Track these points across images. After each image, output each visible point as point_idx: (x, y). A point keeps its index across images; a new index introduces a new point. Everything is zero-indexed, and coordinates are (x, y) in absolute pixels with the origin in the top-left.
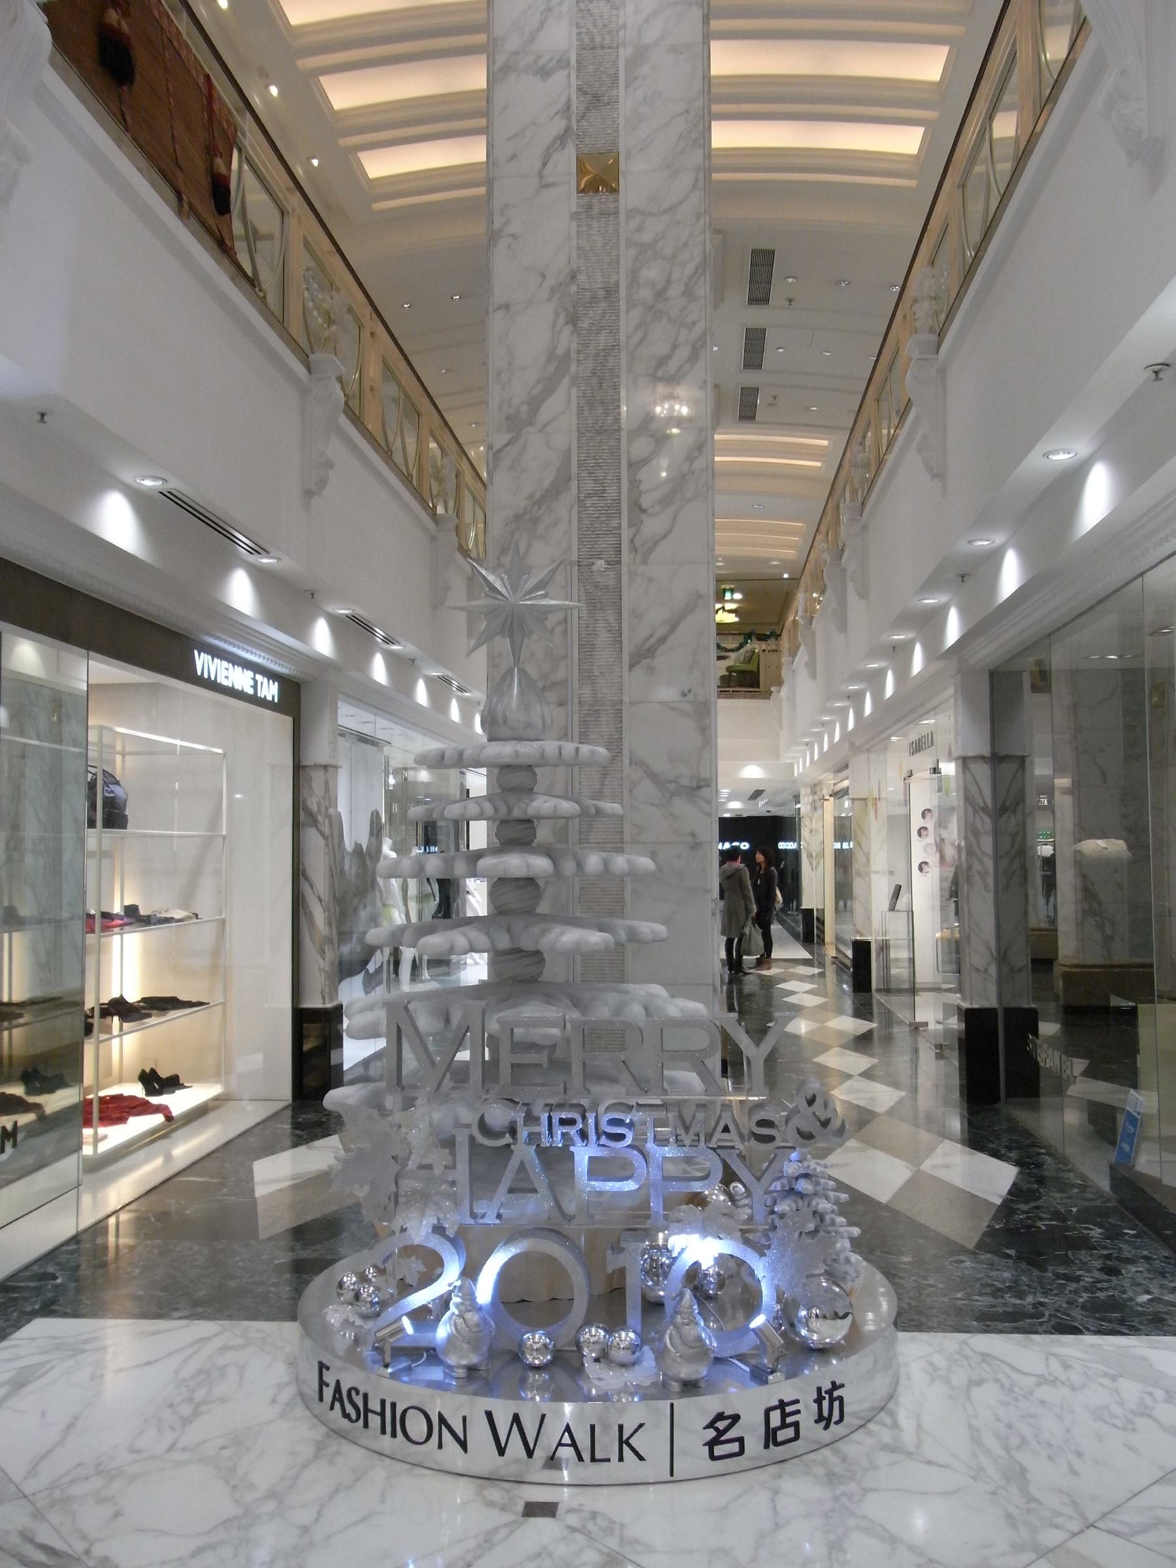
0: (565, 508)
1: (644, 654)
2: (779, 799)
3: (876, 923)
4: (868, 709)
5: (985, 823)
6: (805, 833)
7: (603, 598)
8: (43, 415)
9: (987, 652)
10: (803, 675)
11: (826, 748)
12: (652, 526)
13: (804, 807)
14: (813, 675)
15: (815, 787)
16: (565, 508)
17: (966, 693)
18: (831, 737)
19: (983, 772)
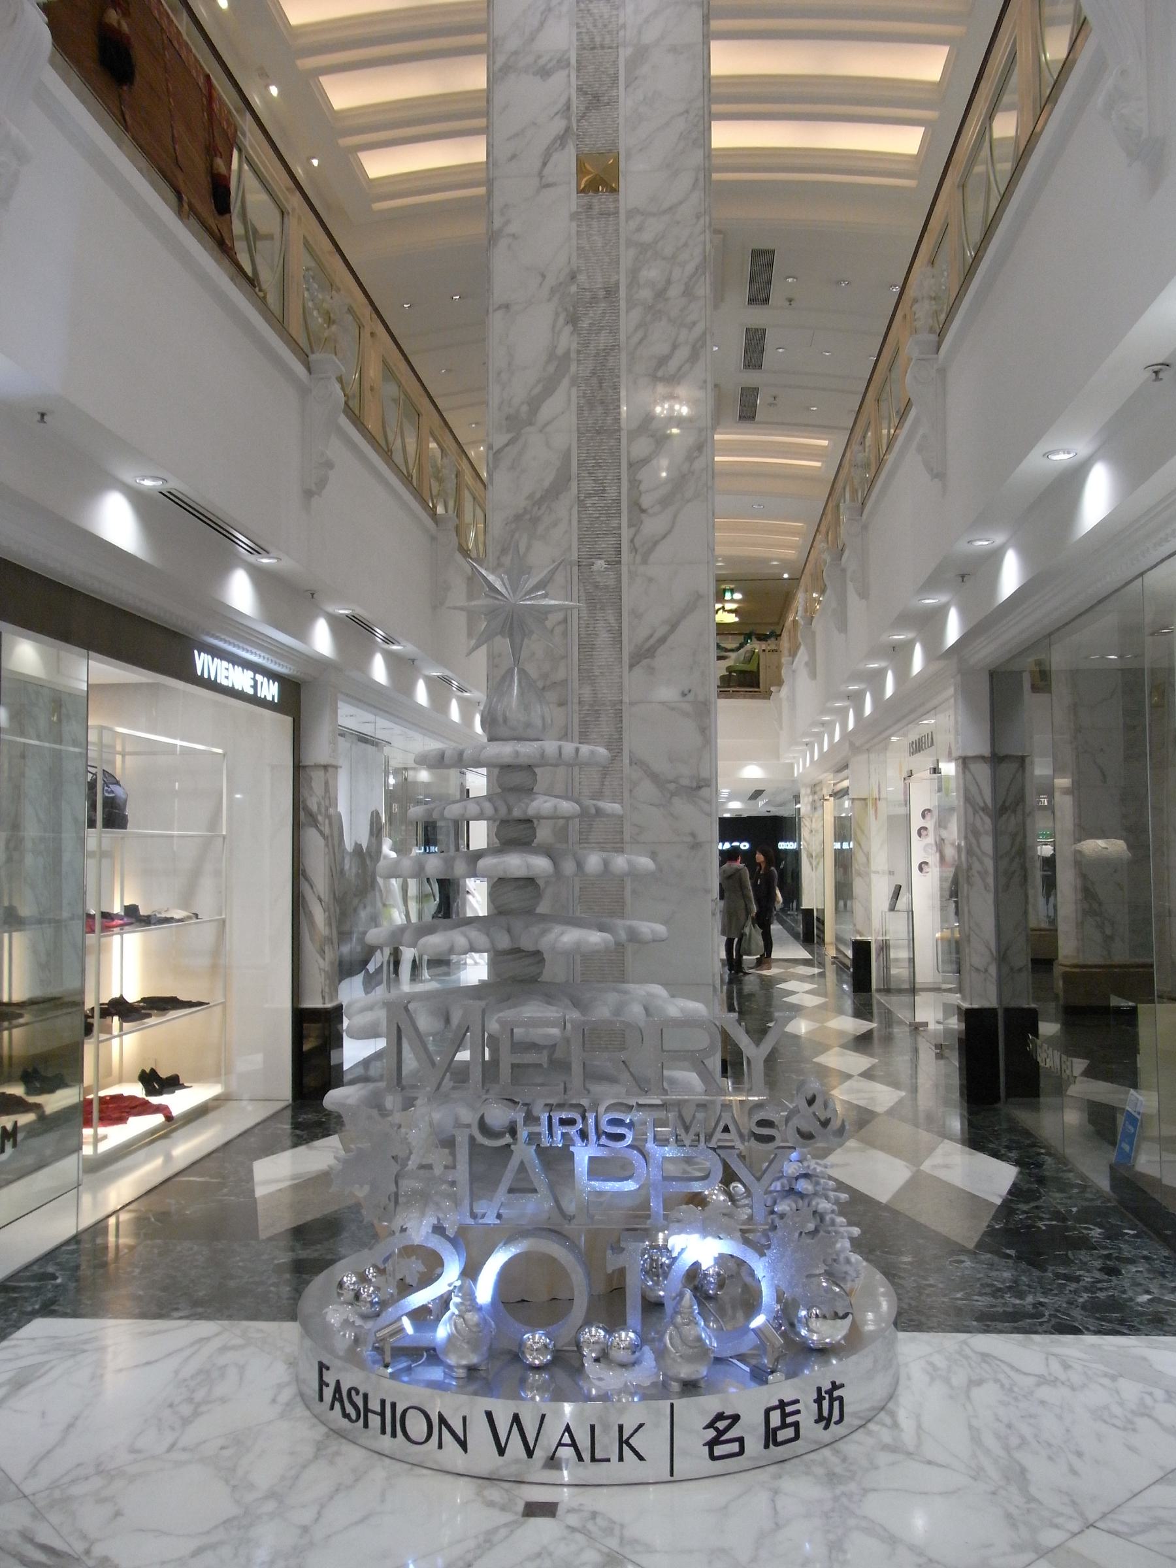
0: (565, 508)
1: (644, 654)
2: (779, 799)
3: (876, 923)
4: (868, 709)
5: (985, 823)
6: (805, 833)
7: (603, 598)
8: (43, 415)
9: (987, 652)
10: (803, 675)
11: (826, 748)
12: (652, 526)
13: (804, 807)
14: (813, 675)
15: (815, 787)
16: (565, 508)
17: (966, 693)
18: (831, 737)
19: (983, 772)
